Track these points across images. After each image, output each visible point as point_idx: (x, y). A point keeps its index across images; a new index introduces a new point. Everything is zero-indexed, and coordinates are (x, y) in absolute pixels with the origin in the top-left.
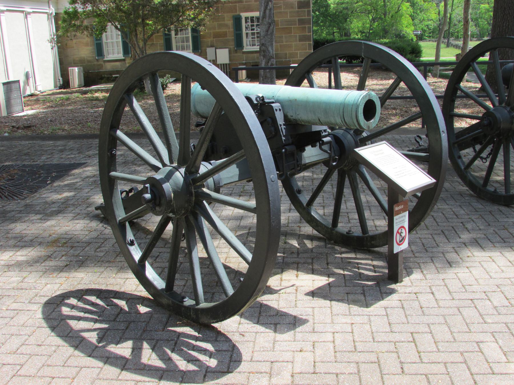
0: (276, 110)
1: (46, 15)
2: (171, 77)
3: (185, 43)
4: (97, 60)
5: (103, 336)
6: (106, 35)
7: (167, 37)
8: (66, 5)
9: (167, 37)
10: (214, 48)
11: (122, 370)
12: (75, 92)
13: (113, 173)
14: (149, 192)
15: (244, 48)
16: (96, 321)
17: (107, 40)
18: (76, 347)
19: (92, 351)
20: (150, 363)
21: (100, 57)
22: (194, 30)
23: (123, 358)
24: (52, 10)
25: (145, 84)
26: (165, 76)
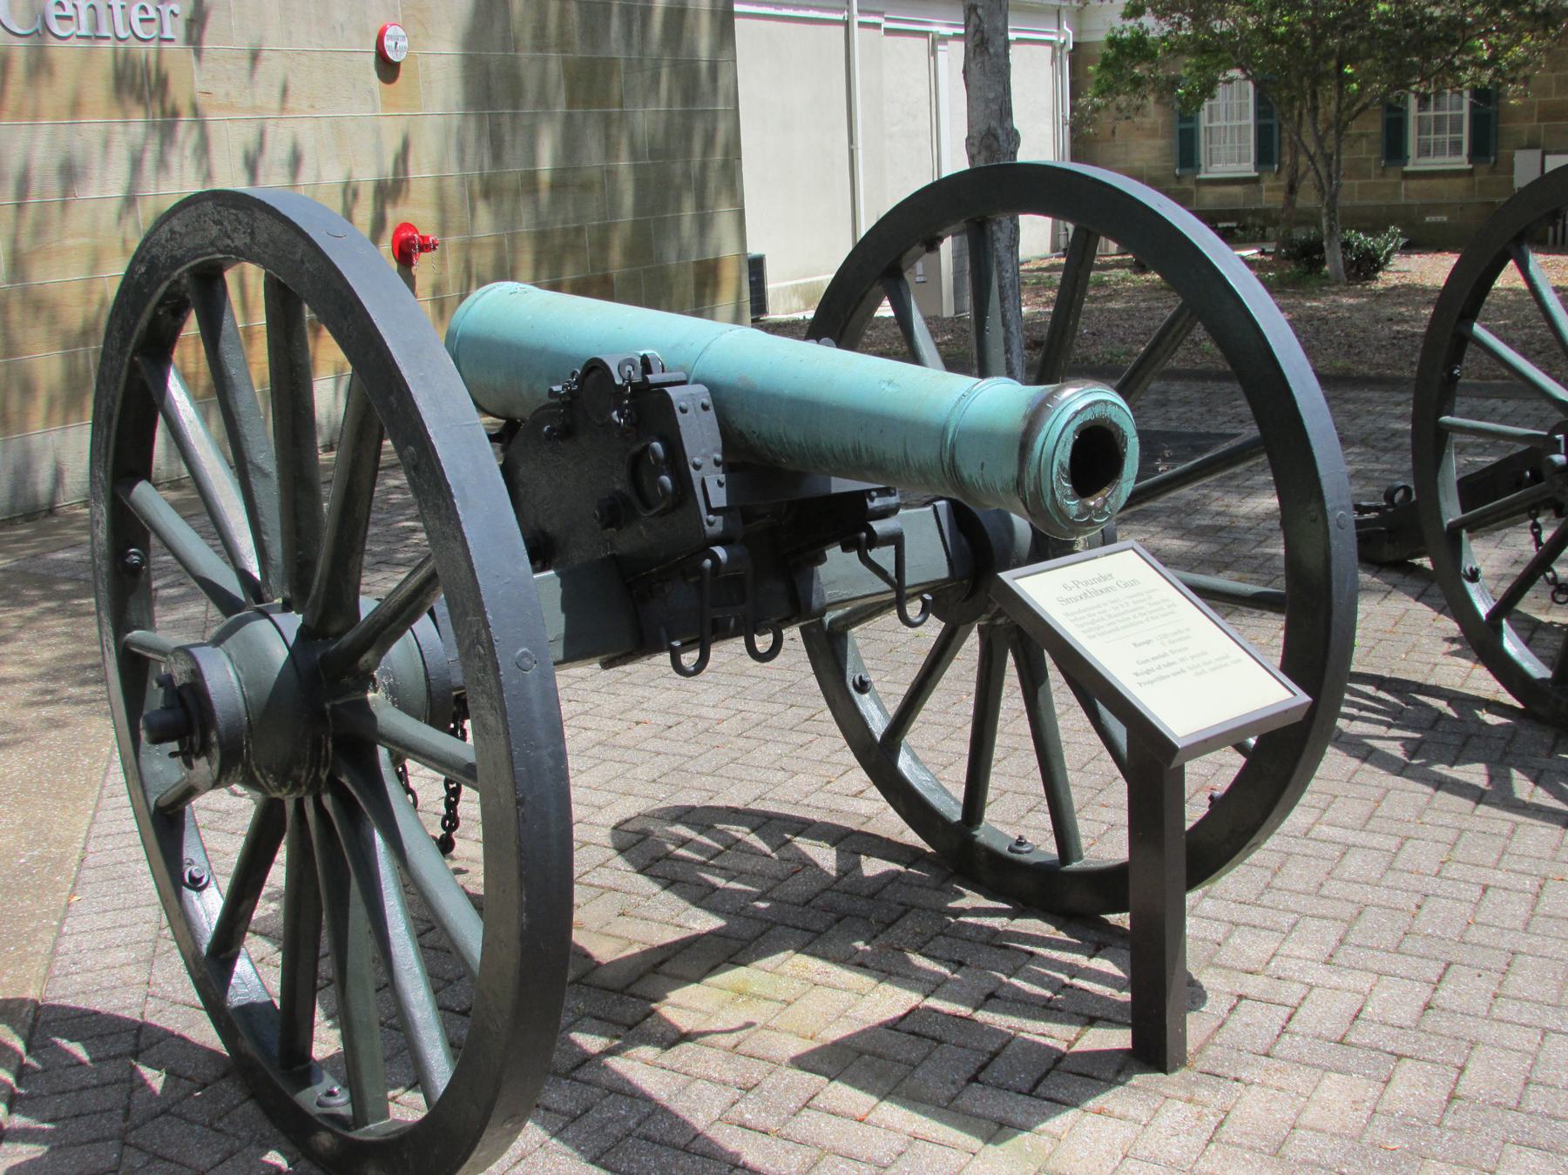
0: (684, 411)
1: (1049, 49)
2: (1402, 235)
3: (1432, 136)
4: (1179, 178)
5: (1413, 749)
6: (1211, 107)
7: (1394, 115)
8: (1110, 20)
9: (1394, 115)
10: (1538, 153)
11: (1478, 803)
12: (1111, 267)
13: (1446, 419)
14: (1563, 449)
15: (1411, 161)
16: (1390, 726)
17: (1211, 120)
18: (1364, 760)
19: (1400, 769)
20: (1535, 800)
21: (1188, 171)
22: (1482, 96)
23: (1475, 787)
24: (1067, 36)
25: (1327, 252)
26: (1386, 230)
